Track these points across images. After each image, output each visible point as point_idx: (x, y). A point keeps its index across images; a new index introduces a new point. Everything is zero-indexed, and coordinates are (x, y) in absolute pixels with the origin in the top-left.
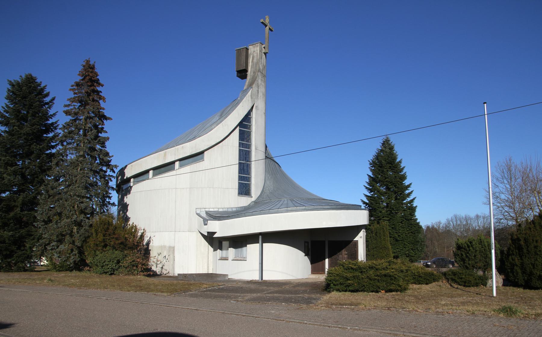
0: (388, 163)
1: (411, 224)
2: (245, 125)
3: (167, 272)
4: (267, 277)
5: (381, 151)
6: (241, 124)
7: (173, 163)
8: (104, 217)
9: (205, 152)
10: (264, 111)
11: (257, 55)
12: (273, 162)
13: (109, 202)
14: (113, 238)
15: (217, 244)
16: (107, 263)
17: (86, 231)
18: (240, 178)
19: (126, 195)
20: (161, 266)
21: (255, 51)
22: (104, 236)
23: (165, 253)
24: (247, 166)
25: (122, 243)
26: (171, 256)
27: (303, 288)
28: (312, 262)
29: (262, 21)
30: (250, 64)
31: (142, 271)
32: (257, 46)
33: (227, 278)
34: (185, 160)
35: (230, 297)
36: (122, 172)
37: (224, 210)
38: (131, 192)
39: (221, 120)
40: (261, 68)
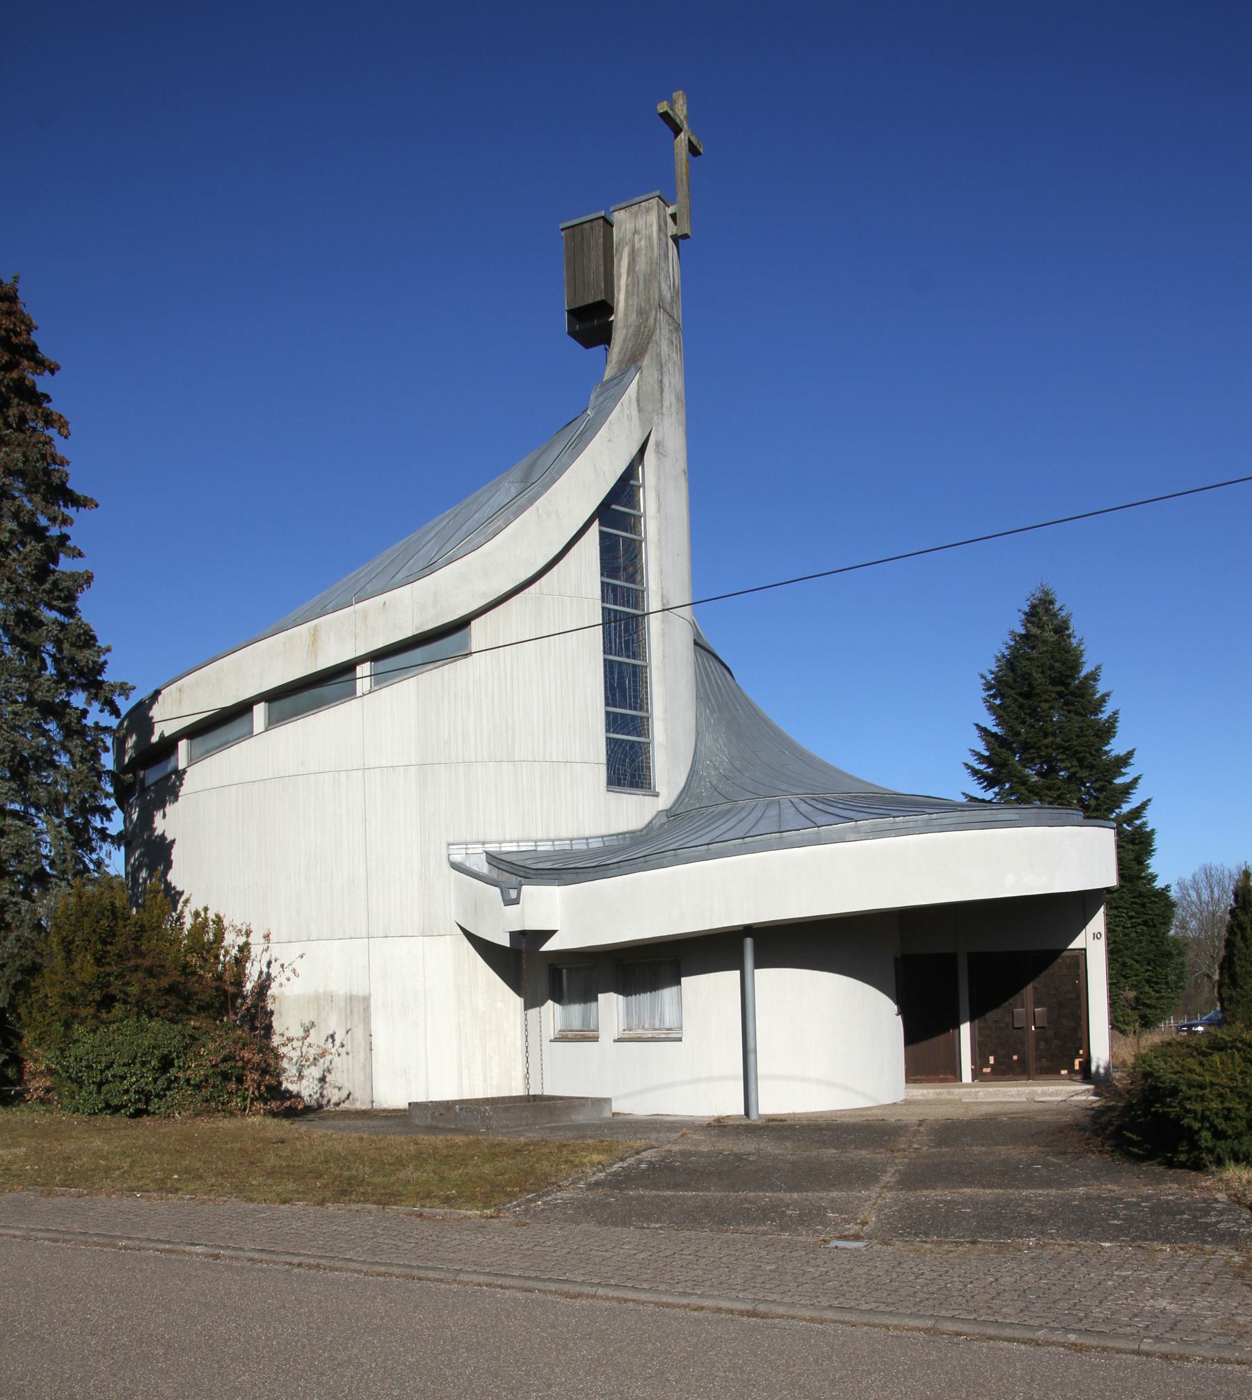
0: (1054, 682)
1: (1141, 895)
2: (617, 512)
3: (344, 1094)
4: (775, 1101)
5: (1026, 637)
6: (604, 513)
7: (347, 669)
8: (89, 888)
9: (475, 624)
10: (682, 464)
11: (650, 246)
12: (717, 664)
13: (103, 830)
14: (136, 968)
15: (544, 983)
16: (117, 1070)
17: (25, 945)
18: (613, 722)
19: (161, 805)
20: (318, 1075)
21: (641, 230)
22: (99, 961)
23: (333, 1023)
24: (635, 674)
25: (172, 990)
26: (359, 1033)
27: (1015, 1153)
28: (911, 1037)
29: (663, 107)
30: (622, 282)
31: (261, 1098)
32: (648, 210)
33: (608, 1114)
34: (395, 657)
35: (810, 1217)
36: (140, 718)
37: (559, 846)
38: (183, 791)
39: (521, 501)
40: (667, 295)
